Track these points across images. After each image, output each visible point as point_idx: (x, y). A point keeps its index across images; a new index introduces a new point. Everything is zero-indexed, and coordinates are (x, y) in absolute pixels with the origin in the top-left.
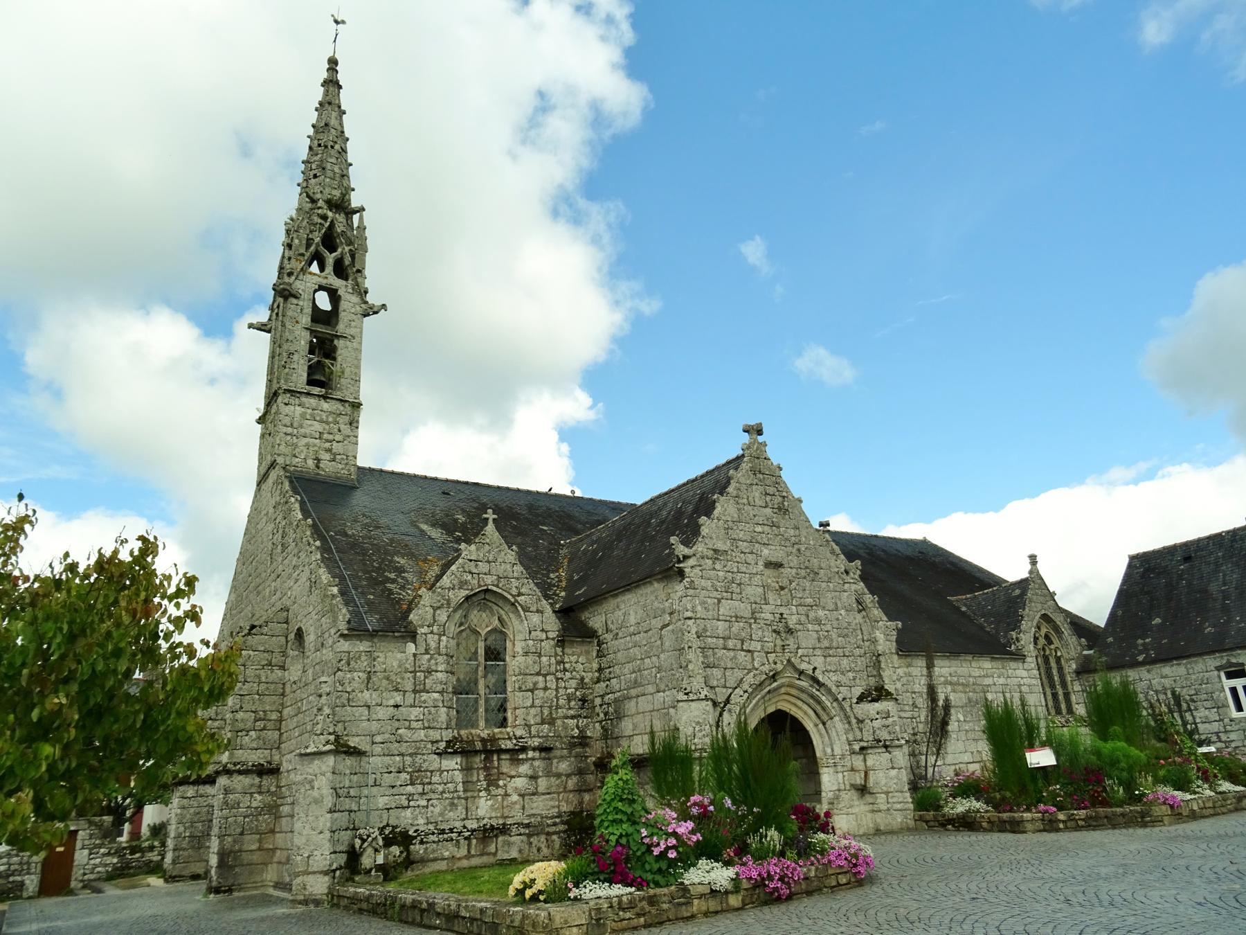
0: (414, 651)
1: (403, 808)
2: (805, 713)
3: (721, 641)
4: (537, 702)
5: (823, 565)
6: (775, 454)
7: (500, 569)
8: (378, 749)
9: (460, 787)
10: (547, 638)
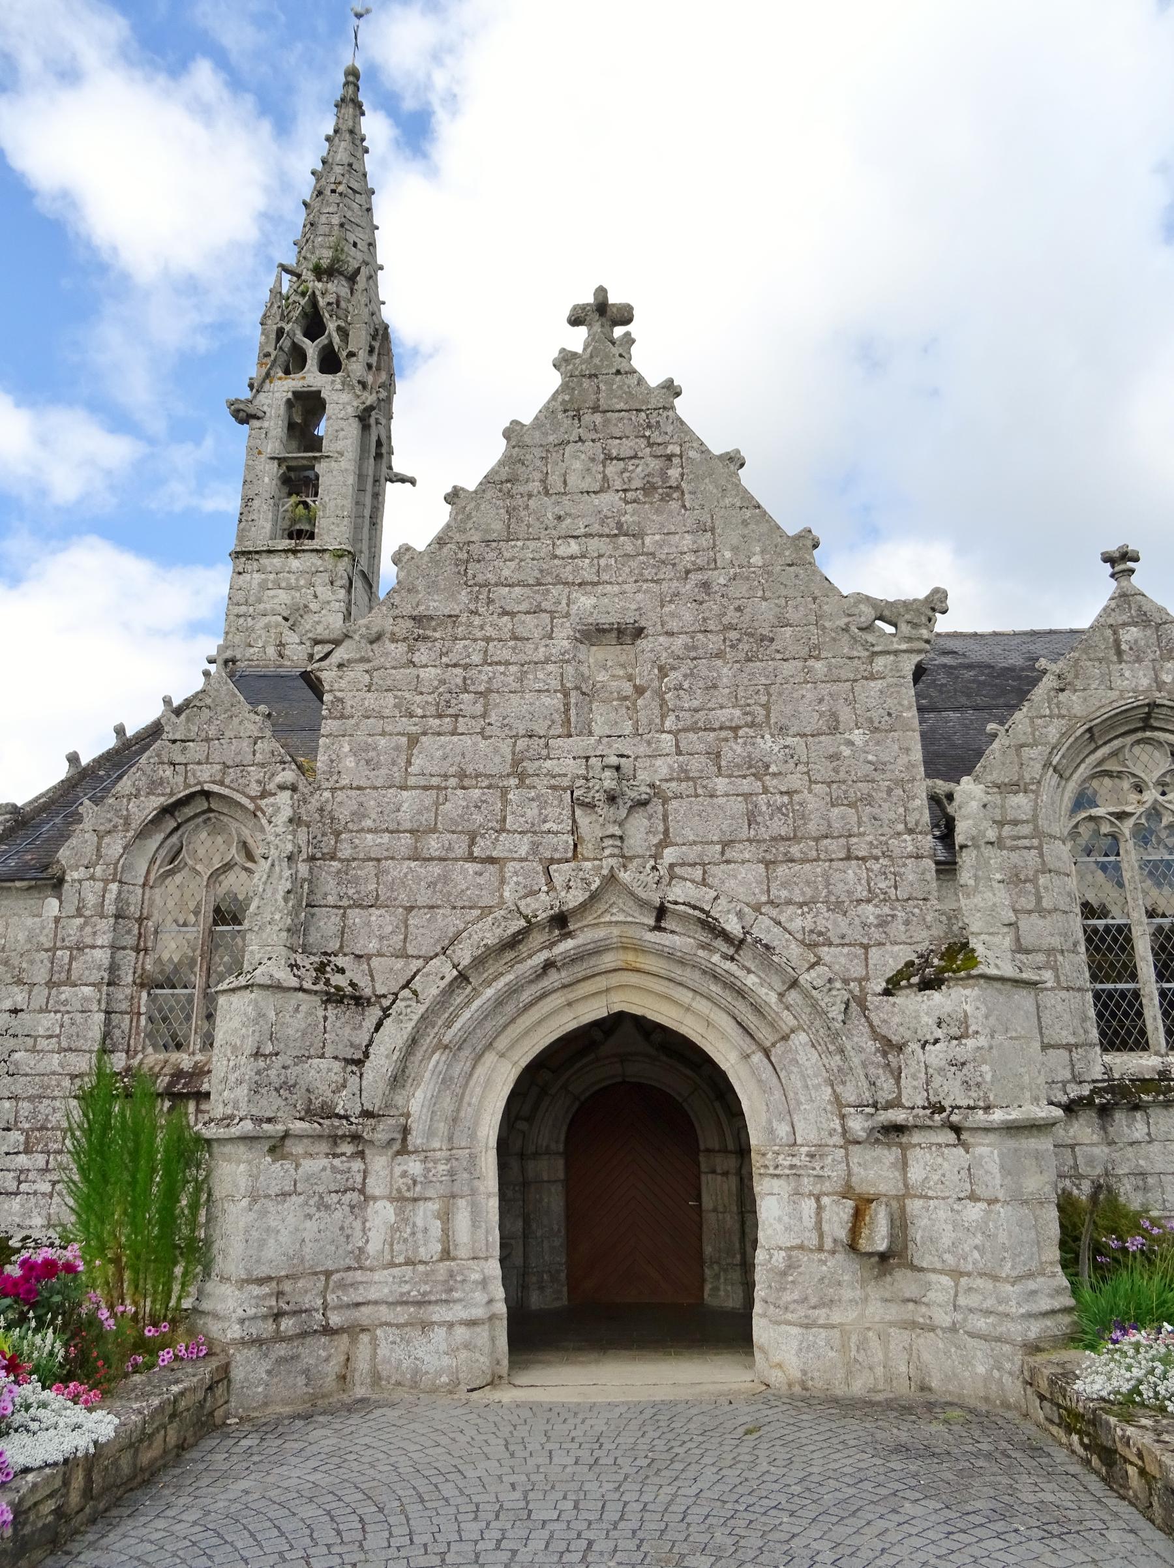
0: (56, 912)
1: (8, 1194)
3: (406, 839)
5: (792, 615)
7: (227, 751)
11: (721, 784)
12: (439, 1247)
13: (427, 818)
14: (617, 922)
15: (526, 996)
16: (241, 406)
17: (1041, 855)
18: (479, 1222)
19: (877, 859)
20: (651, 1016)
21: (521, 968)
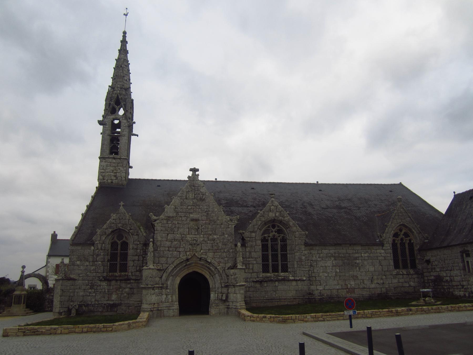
4: (135, 265)
9: (106, 291)
18: (176, 297)
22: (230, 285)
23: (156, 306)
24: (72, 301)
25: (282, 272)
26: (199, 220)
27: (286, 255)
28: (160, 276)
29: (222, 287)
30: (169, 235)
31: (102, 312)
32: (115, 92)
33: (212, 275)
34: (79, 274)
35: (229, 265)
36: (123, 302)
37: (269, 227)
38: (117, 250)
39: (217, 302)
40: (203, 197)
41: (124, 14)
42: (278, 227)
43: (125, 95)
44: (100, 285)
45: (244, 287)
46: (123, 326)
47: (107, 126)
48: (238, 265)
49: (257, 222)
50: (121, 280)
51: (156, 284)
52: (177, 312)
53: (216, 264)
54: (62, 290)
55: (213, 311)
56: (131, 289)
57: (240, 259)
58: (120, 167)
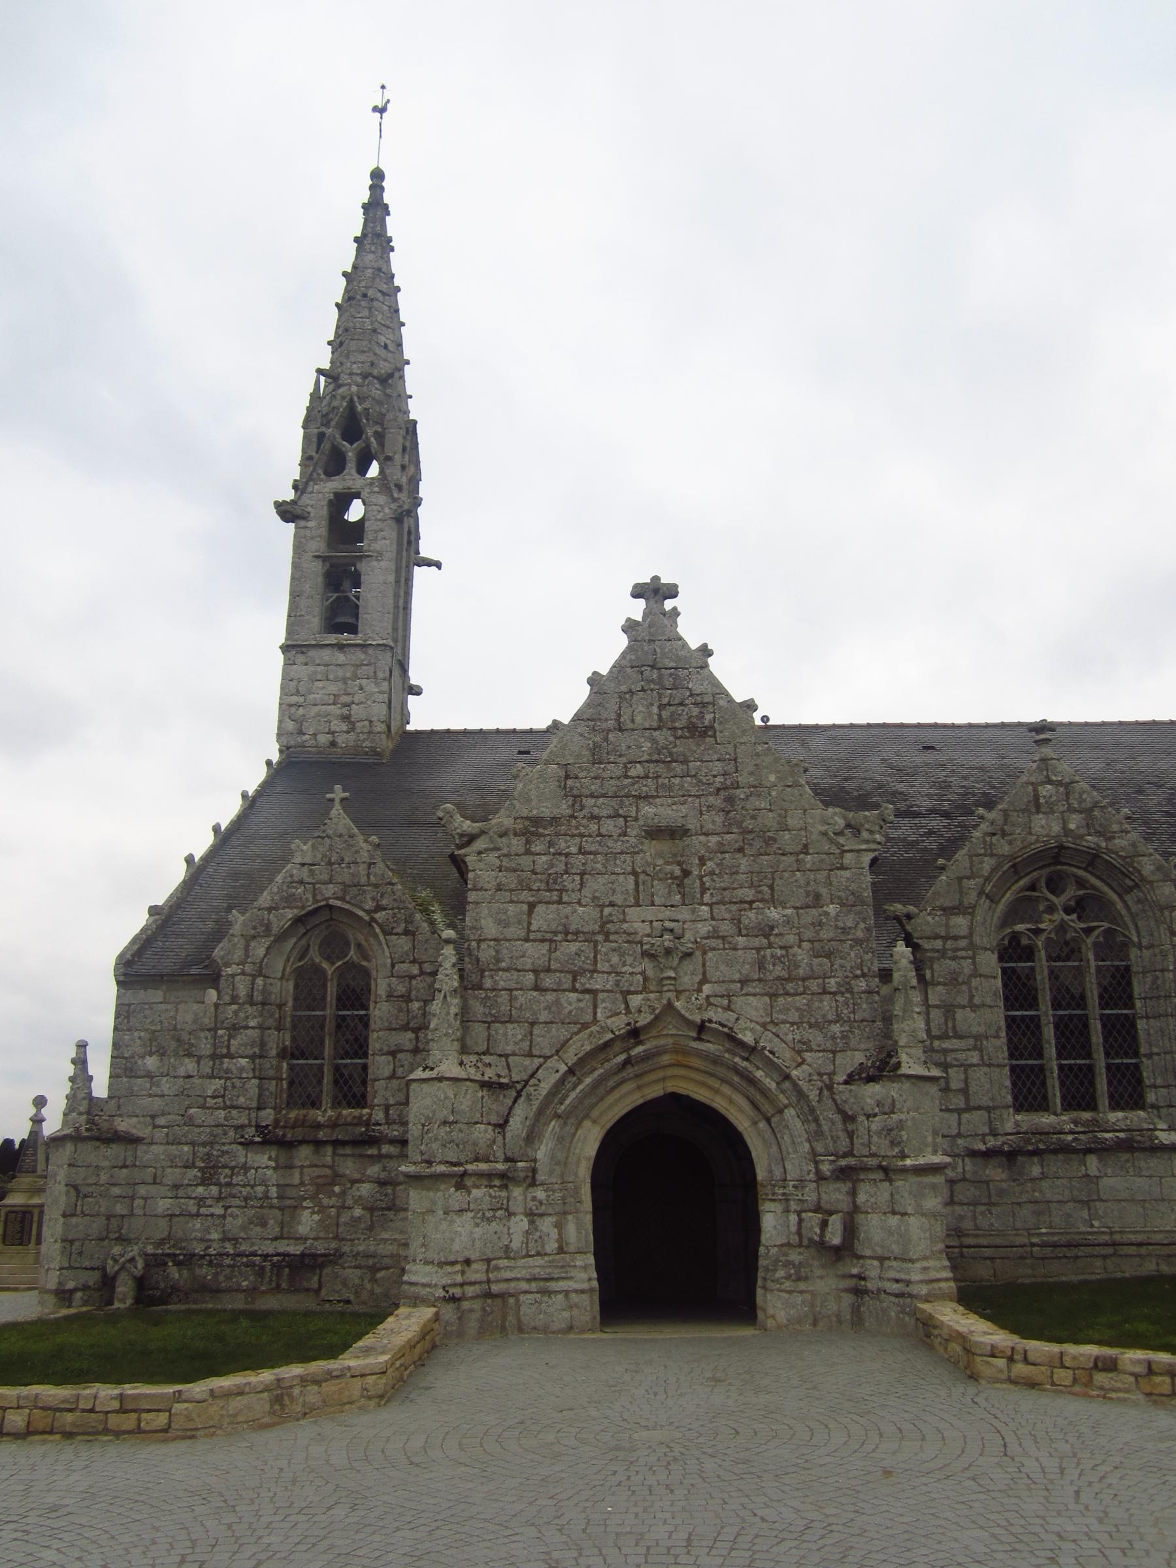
2: (731, 1101)
6: (691, 633)
8: (160, 1135)
9: (273, 1192)
10: (422, 973)
11: (741, 940)
12: (557, 1245)
13: (542, 963)
14: (672, 1035)
15: (611, 1083)
16: (288, 508)
17: (974, 963)
18: (580, 1229)
19: (842, 994)
20: (692, 1095)
21: (607, 1065)
22: (866, 1169)
23: (477, 1272)
24: (122, 1240)
25: (1115, 1106)
26: (685, 832)
27: (1129, 1023)
28: (494, 1119)
29: (820, 1178)
30: (540, 909)
31: (253, 1291)
32: (341, 390)
33: (768, 1115)
34: (153, 1117)
35: (855, 1058)
36: (346, 1249)
37: (1032, 887)
38: (321, 1003)
39: (795, 1256)
40: (701, 716)
41: (375, 109)
42: (1081, 883)
43: (380, 403)
44: (245, 1168)
45: (939, 1179)
46: (236, 1403)
47: (311, 524)
48: (904, 1057)
49: (972, 865)
50: (336, 1143)
51: (477, 1160)
52: (588, 1307)
53: (785, 1056)
54: (76, 1188)
55: (776, 1303)
56: (382, 1183)
57: (911, 1027)
58: (364, 682)
